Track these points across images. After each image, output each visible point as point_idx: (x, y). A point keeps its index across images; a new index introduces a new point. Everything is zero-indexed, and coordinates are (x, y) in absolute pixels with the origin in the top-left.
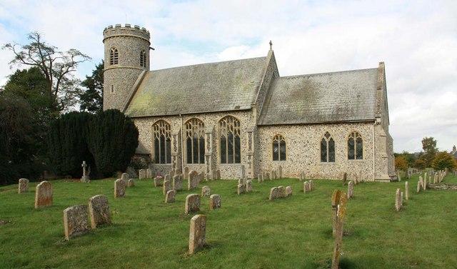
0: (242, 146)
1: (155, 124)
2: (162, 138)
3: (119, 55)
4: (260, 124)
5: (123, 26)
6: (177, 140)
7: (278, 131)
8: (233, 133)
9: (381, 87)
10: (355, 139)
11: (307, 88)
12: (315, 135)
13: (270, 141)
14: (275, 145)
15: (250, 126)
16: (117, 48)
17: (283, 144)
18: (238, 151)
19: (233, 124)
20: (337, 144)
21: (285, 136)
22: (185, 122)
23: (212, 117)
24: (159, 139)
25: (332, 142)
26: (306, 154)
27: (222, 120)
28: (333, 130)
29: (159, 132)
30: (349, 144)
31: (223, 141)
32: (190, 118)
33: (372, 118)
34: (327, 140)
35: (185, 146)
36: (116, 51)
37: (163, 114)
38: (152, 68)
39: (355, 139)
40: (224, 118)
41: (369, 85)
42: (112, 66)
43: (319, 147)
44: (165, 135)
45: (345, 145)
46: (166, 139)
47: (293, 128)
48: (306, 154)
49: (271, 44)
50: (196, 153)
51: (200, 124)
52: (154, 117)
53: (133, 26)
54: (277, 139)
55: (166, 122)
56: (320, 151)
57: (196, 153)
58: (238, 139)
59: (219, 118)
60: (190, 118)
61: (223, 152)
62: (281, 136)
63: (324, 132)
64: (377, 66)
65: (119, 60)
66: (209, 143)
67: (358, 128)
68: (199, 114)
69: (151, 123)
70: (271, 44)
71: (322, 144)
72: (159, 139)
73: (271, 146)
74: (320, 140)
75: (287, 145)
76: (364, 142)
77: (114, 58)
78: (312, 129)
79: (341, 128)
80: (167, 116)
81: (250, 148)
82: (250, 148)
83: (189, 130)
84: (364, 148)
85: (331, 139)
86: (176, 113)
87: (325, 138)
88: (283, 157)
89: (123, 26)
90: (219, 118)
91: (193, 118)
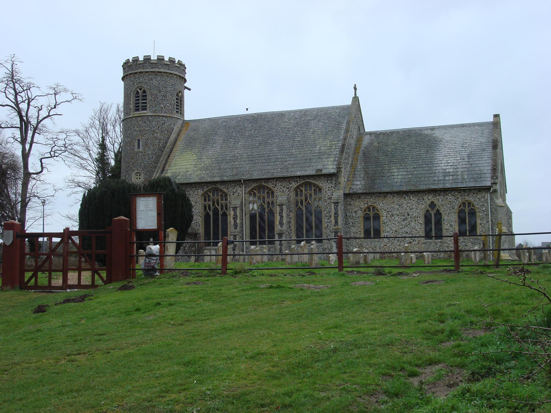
0: (325, 220)
1: (206, 193)
2: (216, 210)
3: (149, 98)
4: (347, 192)
5: (154, 57)
6: (238, 214)
7: (371, 201)
8: (266, 206)
9: (496, 145)
10: (467, 210)
11: (417, 142)
12: (417, 208)
13: (360, 214)
14: (367, 218)
15: (335, 196)
16: (145, 87)
17: (377, 217)
18: (319, 226)
19: (266, 194)
20: (445, 217)
21: (379, 207)
22: (248, 190)
23: (285, 184)
24: (211, 213)
25: (438, 214)
26: (406, 229)
27: (298, 187)
28: (440, 201)
29: (211, 203)
30: (459, 217)
31: (253, 217)
32: (255, 185)
33: (488, 184)
34: (433, 213)
35: (248, 222)
36: (144, 92)
37: (217, 179)
38: (188, 116)
39: (467, 210)
40: (301, 185)
41: (484, 139)
42: (137, 113)
43: (422, 220)
44: (219, 208)
45: (454, 217)
46: (220, 213)
47: (389, 198)
48: (406, 229)
49: (355, 89)
50: (262, 230)
51: (268, 193)
52: (299, 177)
53: (166, 59)
54: (369, 211)
55: (221, 191)
56: (423, 226)
57: (262, 230)
58: (225, 215)
59: (294, 185)
60: (255, 185)
61: (299, 228)
62: (374, 208)
63: (429, 202)
64: (491, 119)
65: (148, 105)
66: (282, 217)
67: (471, 198)
68: (267, 180)
69: (201, 192)
70: (355, 89)
71: (426, 217)
72: (211, 213)
73: (361, 220)
74: (423, 213)
75: (383, 219)
76: (478, 214)
77: (141, 101)
78: (413, 200)
79: (450, 197)
80: (223, 182)
81: (336, 222)
82: (336, 222)
83: (207, 203)
84: (478, 222)
85: (438, 210)
86: (236, 178)
87: (430, 209)
88: (377, 234)
89: (154, 57)
90: (294, 185)
91: (260, 186)
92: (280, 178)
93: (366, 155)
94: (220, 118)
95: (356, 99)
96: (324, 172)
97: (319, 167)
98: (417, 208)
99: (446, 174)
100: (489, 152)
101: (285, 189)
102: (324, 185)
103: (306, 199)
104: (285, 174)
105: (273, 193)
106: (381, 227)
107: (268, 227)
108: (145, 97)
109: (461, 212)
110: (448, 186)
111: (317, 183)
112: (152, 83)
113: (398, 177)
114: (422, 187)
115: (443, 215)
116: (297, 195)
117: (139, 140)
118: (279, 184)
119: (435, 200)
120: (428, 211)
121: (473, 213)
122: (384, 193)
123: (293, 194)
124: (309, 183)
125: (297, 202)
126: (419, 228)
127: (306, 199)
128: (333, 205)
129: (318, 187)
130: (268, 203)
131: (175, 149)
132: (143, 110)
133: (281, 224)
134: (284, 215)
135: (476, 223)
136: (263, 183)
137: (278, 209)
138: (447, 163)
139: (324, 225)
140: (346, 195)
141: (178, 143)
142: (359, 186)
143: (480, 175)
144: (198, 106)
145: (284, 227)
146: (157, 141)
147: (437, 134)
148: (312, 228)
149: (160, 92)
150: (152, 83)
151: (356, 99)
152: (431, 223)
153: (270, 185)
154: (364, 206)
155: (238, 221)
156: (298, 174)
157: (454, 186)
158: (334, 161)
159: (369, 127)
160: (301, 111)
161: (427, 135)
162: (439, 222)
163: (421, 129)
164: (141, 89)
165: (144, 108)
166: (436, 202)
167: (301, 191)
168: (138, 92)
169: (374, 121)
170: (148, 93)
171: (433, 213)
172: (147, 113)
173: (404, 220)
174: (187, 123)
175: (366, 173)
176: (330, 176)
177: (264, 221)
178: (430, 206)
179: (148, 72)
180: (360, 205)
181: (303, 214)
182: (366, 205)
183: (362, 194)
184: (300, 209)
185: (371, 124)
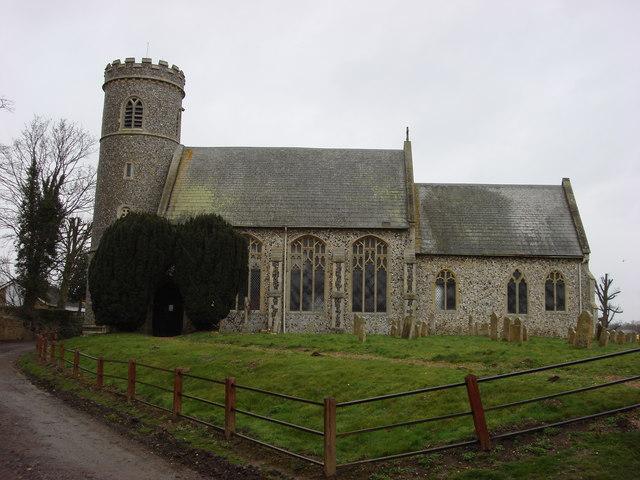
2: (370, 266)
3: (146, 112)
7: (445, 264)
8: (313, 262)
10: (555, 281)
12: (499, 274)
20: (531, 288)
23: (341, 236)
25: (523, 284)
26: (486, 300)
27: (357, 242)
30: (547, 289)
31: (295, 274)
36: (139, 103)
37: (249, 224)
39: (555, 281)
40: (361, 240)
42: (128, 130)
43: (505, 291)
45: (542, 289)
47: (468, 263)
48: (486, 300)
52: (361, 229)
54: (443, 276)
59: (353, 239)
61: (357, 292)
62: (448, 273)
63: (513, 270)
66: (339, 277)
67: (560, 268)
68: (318, 230)
71: (509, 287)
75: (459, 286)
77: (134, 115)
78: (495, 266)
79: (537, 266)
81: (410, 288)
82: (410, 288)
84: (567, 295)
85: (523, 280)
86: (276, 225)
90: (353, 239)
91: (308, 236)
92: (335, 229)
93: (427, 209)
94: (300, 149)
95: (408, 144)
96: (393, 225)
97: (385, 220)
98: (499, 274)
99: (529, 240)
100: (567, 220)
101: (340, 243)
102: (392, 241)
103: (367, 257)
104: (342, 225)
105: (323, 246)
106: (457, 296)
107: (316, 289)
108: (140, 110)
109: (549, 284)
110: (536, 253)
111: (380, 237)
112: (140, 95)
113: (473, 237)
114: (508, 253)
115: (529, 287)
116: (355, 251)
117: (129, 165)
118: (333, 237)
119: (519, 267)
120: (512, 280)
121: (561, 285)
122: (461, 256)
123: (350, 249)
124: (370, 236)
125: (355, 260)
126: (502, 299)
127: (367, 257)
128: (406, 268)
129: (383, 242)
130: (317, 259)
131: (178, 181)
132: (136, 126)
133: (338, 286)
134: (342, 274)
135: (564, 296)
136: (312, 234)
137: (335, 267)
138: (526, 225)
139: (390, 290)
140: (417, 255)
141: (181, 173)
142: (430, 245)
143: (566, 245)
144: (204, 125)
145: (342, 290)
146: (154, 169)
147: (504, 193)
148: (373, 293)
149: (160, 106)
150: (140, 95)
151: (408, 144)
152: (515, 294)
153: (321, 237)
154: (437, 270)
155: (280, 279)
156: (361, 225)
157: (543, 253)
158: (402, 213)
159: (419, 178)
160: (341, 151)
161: (493, 194)
162: (524, 295)
163: (482, 186)
164: (134, 100)
165: (139, 125)
166: (521, 270)
167: (361, 246)
168: (130, 103)
169: (425, 172)
170: (145, 106)
171: (518, 282)
172: (143, 130)
173: (485, 289)
174: (188, 151)
175: (435, 232)
176: (398, 231)
177: (310, 281)
178: (514, 274)
179: (147, 79)
180: (433, 268)
181: (361, 275)
182: (440, 269)
183: (436, 255)
184: (358, 268)
185: (425, 172)
